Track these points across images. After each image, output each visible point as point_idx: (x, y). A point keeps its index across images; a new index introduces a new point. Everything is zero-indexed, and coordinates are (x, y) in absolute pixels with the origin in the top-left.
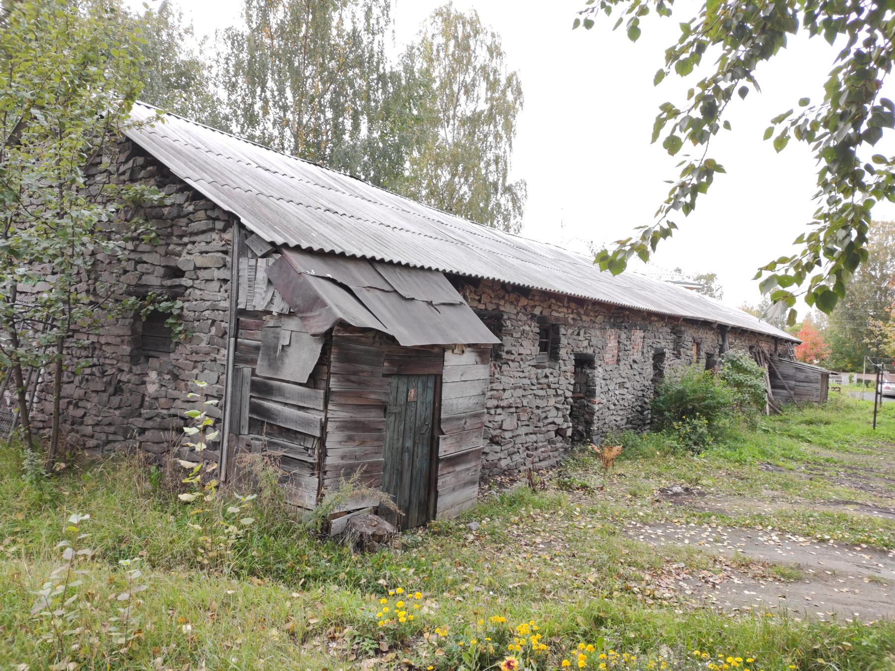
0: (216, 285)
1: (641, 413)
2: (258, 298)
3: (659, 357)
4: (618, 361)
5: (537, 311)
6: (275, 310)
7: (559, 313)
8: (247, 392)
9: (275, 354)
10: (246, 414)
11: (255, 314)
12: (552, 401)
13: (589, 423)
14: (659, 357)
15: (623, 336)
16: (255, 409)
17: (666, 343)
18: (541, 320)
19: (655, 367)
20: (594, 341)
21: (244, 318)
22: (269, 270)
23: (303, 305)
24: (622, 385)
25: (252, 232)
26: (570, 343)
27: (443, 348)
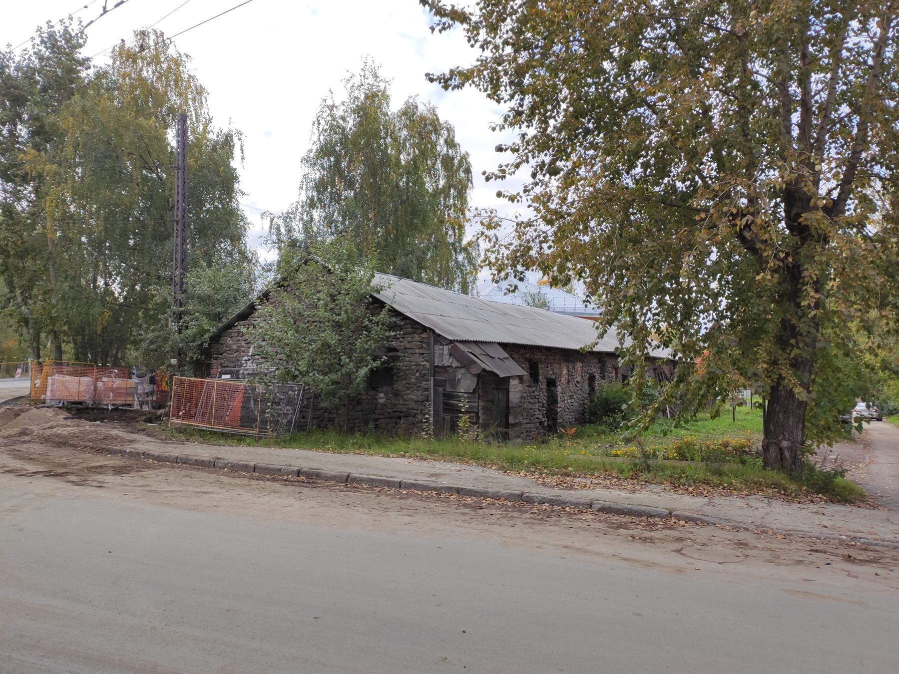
0: (417, 355)
1: (583, 414)
2: (447, 361)
3: (592, 378)
4: (569, 382)
5: (528, 356)
6: (454, 366)
7: (538, 356)
8: (441, 398)
9: (455, 383)
10: (442, 406)
11: (444, 367)
12: (537, 406)
13: (555, 419)
14: (592, 378)
15: (571, 366)
16: (445, 404)
17: (595, 370)
18: (530, 361)
19: (590, 385)
20: (555, 371)
21: (437, 370)
22: (449, 350)
23: (467, 364)
24: (571, 397)
25: (439, 335)
26: (544, 373)
27: (509, 377)
